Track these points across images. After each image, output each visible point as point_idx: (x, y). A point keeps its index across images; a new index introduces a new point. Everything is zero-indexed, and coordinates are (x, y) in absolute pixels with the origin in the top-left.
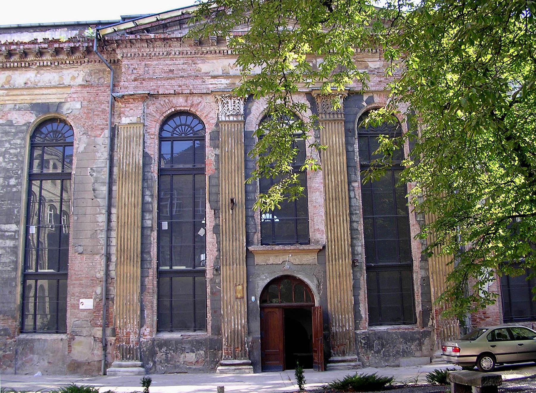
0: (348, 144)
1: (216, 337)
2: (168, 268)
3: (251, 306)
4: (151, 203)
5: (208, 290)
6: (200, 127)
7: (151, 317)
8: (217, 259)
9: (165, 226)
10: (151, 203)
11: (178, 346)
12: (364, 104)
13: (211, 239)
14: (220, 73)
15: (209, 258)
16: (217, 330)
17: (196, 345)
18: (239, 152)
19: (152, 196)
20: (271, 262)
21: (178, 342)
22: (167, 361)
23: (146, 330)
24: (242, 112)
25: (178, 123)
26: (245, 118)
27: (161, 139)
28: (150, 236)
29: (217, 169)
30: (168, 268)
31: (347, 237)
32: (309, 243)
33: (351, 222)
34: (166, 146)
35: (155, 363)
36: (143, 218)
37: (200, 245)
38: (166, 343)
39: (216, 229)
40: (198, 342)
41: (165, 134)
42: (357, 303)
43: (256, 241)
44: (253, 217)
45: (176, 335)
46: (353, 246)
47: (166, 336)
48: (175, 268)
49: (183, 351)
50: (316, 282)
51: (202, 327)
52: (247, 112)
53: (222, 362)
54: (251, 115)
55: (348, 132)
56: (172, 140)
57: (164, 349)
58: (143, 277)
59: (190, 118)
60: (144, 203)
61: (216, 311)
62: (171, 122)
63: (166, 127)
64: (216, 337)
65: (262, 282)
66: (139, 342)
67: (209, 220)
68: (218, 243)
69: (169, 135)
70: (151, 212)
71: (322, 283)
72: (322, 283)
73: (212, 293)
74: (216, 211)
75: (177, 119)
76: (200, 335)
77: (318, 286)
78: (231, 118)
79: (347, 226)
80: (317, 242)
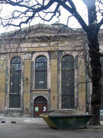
0: (58, 64)
1: (22, 110)
2: (12, 94)
3: (31, 103)
4: (8, 78)
5: (21, 99)
6: (46, 59)
7: (8, 104)
8: (23, 92)
9: (12, 84)
10: (8, 78)
11: (14, 111)
12: (63, 54)
13: (22, 87)
14: (25, 47)
15: (22, 91)
16: (23, 108)
17: (18, 111)
18: (29, 66)
19: (8, 77)
20: (37, 93)
21: (14, 110)
22: (11, 114)
23: (6, 107)
24: (31, 56)
25: (41, 58)
26: (31, 58)
27: (11, 64)
28: (7, 86)
29: (24, 71)
30: (12, 94)
31: (56, 88)
32: (47, 89)
33: (58, 83)
34: (37, 64)
35: (8, 115)
36: (6, 82)
37: (19, 88)
38: (11, 110)
39: (23, 85)
40: (18, 110)
41: (37, 61)
42: (58, 103)
43: (33, 88)
44: (32, 82)
45: (13, 109)
46: (58, 89)
47: (11, 109)
48: (14, 94)
49: (15, 112)
50: (48, 98)
51: (20, 107)
52: (32, 57)
53: (24, 115)
54: (33, 57)
55: (58, 61)
56: (38, 63)
57: (10, 112)
58: (6, 95)
59: (43, 57)
60: (6, 78)
61: (23, 104)
62: (38, 58)
63: (37, 60)
64: (22, 110)
65: (34, 97)
66: (4, 110)
67: (22, 83)
68: (24, 88)
69: (38, 61)
70: (8, 80)
71: (49, 98)
72: (49, 98)
73: (22, 99)
74: (23, 81)
75: (40, 58)
76: (19, 109)
77: (48, 99)
78: (28, 58)
79: (56, 85)
80: (49, 88)
